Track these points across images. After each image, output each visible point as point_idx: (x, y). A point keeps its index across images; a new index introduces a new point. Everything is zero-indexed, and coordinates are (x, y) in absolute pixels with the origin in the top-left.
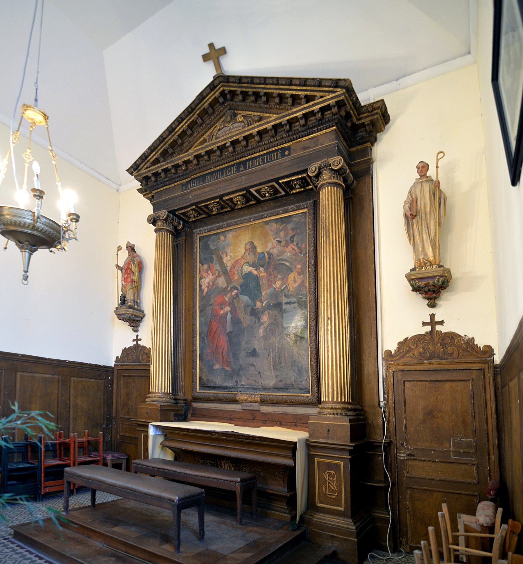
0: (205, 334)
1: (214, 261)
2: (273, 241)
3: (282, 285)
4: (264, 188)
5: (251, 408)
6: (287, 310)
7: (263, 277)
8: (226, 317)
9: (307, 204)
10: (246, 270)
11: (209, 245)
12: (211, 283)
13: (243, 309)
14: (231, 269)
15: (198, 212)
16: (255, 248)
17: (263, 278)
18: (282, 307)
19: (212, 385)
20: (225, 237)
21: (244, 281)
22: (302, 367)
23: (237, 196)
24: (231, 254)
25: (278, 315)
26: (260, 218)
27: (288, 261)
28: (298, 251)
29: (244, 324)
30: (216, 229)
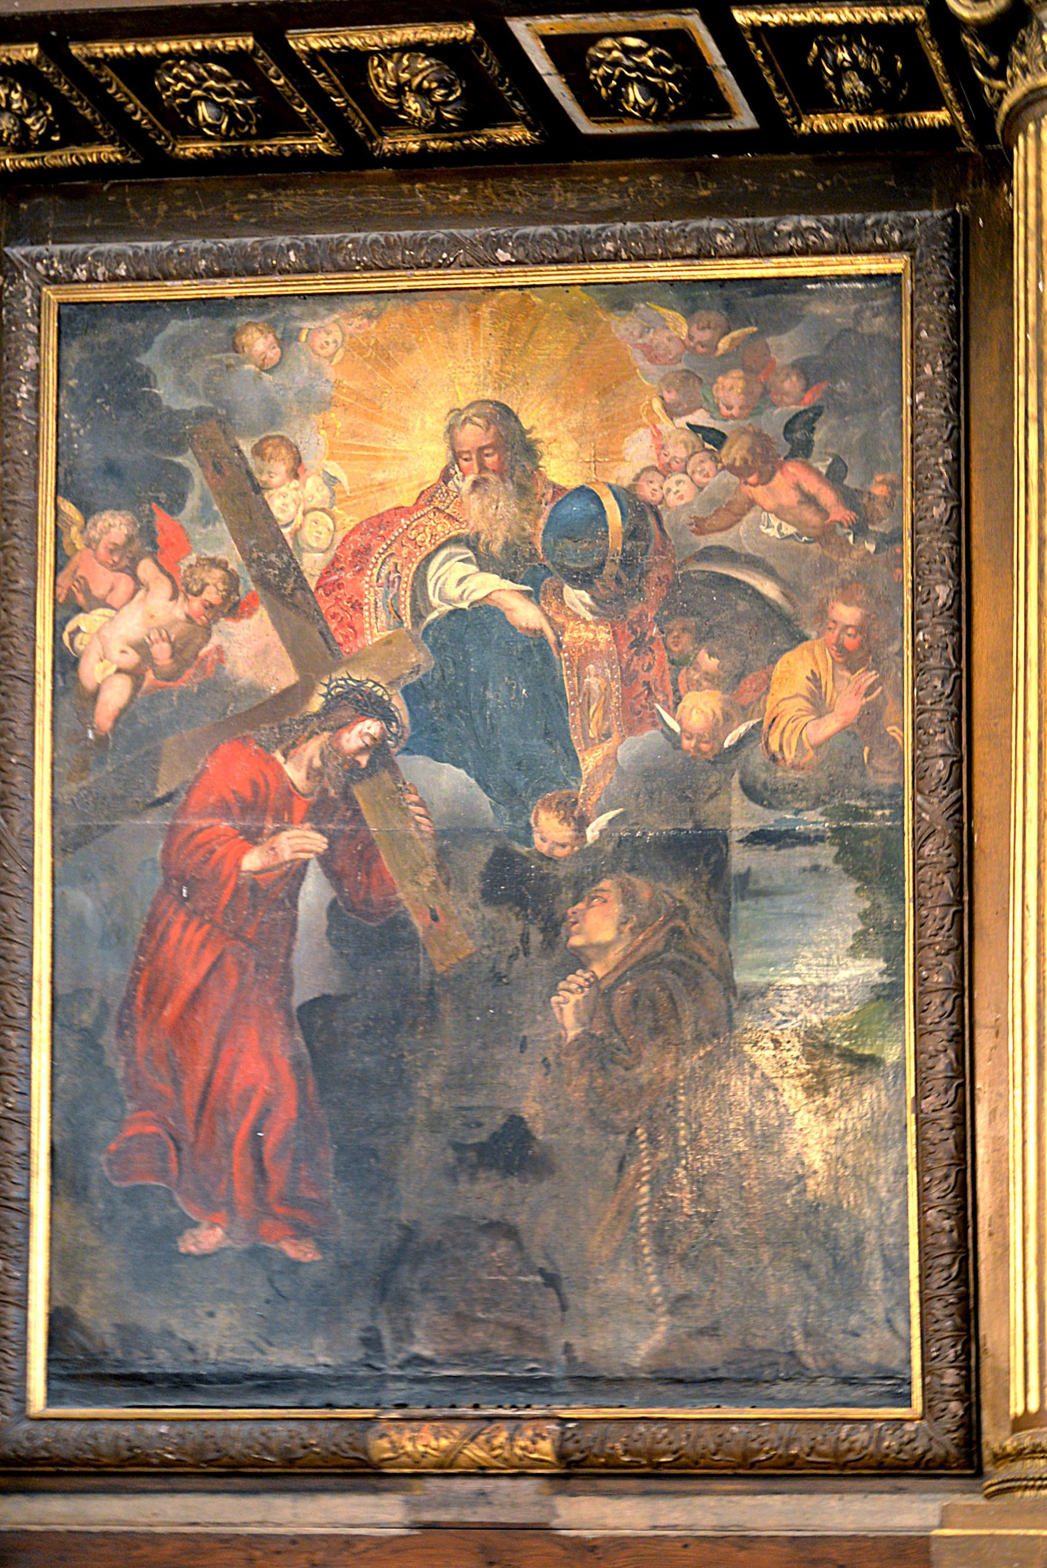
0: (104, 1005)
1: (193, 501)
2: (666, 425)
3: (728, 720)
4: (615, 35)
5: (481, 1515)
6: (763, 883)
7: (586, 655)
8: (293, 896)
9: (909, 225)
10: (453, 592)
11: (146, 379)
12: (162, 652)
13: (428, 850)
14: (333, 566)
15: (62, 106)
16: (530, 450)
17: (585, 659)
18: (723, 863)
19: (165, 1361)
20: (286, 340)
21: (441, 667)
22: (859, 1241)
23: (406, 48)
24: (334, 468)
25: (694, 908)
26: (566, 252)
27: (770, 573)
28: (839, 513)
29: (436, 954)
30: (210, 274)
